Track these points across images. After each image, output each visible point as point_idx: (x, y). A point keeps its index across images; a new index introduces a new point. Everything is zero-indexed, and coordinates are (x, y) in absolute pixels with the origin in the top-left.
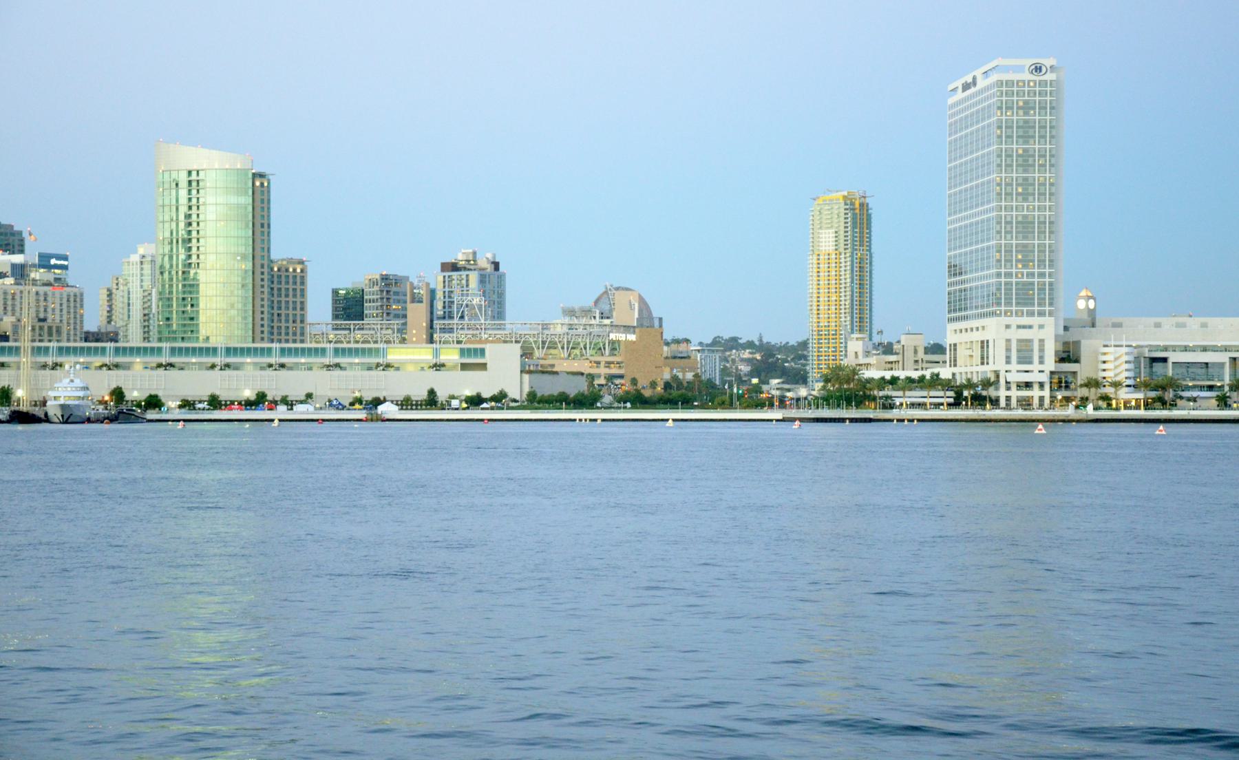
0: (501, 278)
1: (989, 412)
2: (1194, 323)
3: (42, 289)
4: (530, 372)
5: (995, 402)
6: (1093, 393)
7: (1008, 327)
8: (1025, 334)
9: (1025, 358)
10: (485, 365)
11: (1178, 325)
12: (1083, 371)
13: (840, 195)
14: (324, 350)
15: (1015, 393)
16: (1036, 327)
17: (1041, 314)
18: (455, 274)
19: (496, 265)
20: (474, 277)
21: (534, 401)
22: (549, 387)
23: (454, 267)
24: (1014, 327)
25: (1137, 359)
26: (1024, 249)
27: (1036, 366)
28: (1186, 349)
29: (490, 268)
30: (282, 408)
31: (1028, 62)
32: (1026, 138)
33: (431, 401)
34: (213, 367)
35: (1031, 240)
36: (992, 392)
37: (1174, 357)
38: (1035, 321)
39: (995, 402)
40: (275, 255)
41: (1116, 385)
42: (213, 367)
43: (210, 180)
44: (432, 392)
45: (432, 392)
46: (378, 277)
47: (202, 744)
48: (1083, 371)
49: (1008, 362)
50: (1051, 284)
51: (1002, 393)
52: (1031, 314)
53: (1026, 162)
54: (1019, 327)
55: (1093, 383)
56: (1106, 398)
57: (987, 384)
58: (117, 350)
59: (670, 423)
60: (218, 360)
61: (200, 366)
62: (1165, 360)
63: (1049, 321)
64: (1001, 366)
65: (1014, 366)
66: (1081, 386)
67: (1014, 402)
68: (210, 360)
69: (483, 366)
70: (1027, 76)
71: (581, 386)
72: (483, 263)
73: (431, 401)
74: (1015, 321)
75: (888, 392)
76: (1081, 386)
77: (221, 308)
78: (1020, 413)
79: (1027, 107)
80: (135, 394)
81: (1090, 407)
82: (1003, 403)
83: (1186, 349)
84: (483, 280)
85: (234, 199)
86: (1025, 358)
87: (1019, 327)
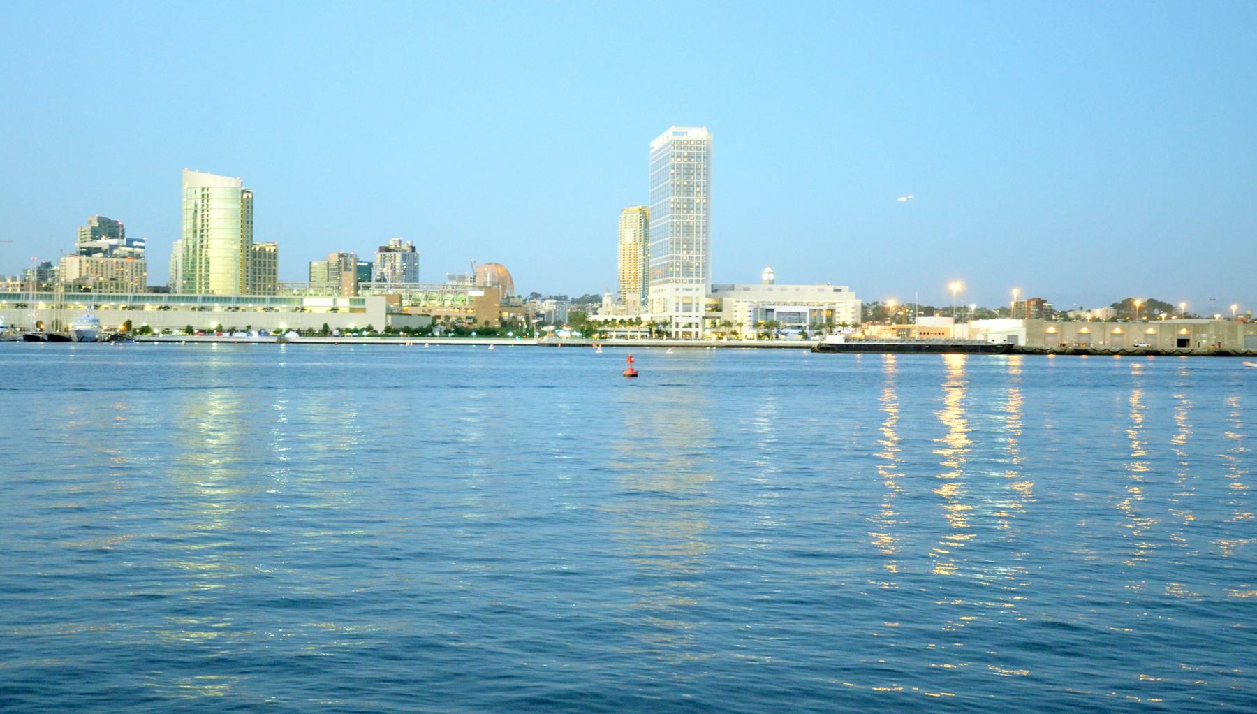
0: (416, 259)
1: (665, 341)
2: (791, 288)
3: (120, 260)
4: (392, 314)
5: (669, 335)
6: (728, 330)
9: (687, 308)
10: (364, 310)
11: (783, 290)
12: (725, 316)
13: (637, 208)
14: (126, 298)
15: (681, 330)
17: (697, 282)
18: (388, 254)
19: (413, 249)
20: (399, 256)
21: (390, 331)
22: (403, 322)
23: (387, 250)
25: (756, 309)
26: (688, 243)
27: (694, 313)
28: (785, 304)
29: (409, 250)
30: (227, 334)
32: (688, 175)
33: (326, 331)
34: (193, 309)
35: (692, 236)
36: (668, 329)
37: (777, 309)
38: (694, 286)
39: (669, 335)
41: (741, 325)
42: (193, 309)
43: (214, 193)
44: (326, 326)
45: (326, 326)
47: (363, 608)
48: (725, 316)
51: (673, 330)
52: (691, 282)
53: (689, 189)
55: (728, 324)
56: (735, 333)
57: (665, 324)
58: (169, 298)
59: (491, 347)
60: (197, 305)
61: (186, 307)
62: (772, 310)
63: (702, 286)
64: (674, 314)
65: (681, 313)
67: (680, 335)
68: (193, 305)
69: (364, 310)
71: (426, 322)
72: (405, 247)
73: (326, 331)
74: (681, 286)
75: (606, 328)
77: (223, 273)
78: (683, 342)
79: (690, 157)
80: (136, 325)
81: (725, 338)
82: (674, 335)
84: (404, 258)
85: (230, 206)
86: (687, 308)
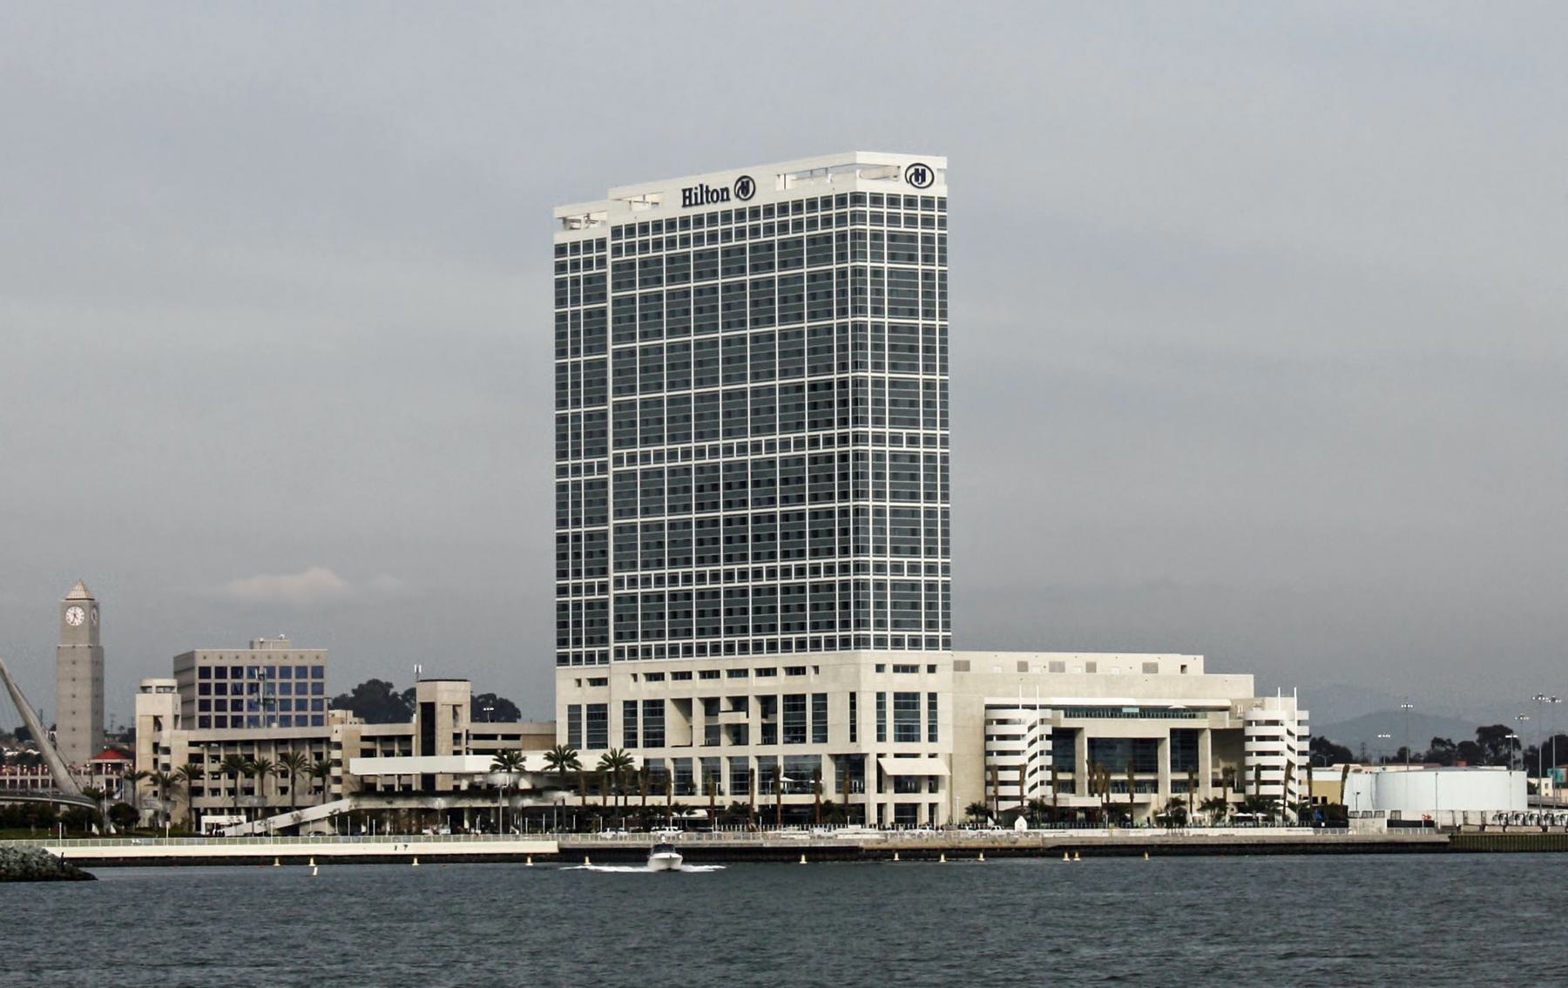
7: (880, 668)
8: (906, 683)
16: (923, 669)
17: (932, 643)
24: (889, 669)
31: (905, 160)
38: (922, 657)
40: (1251, 677)
46: (1474, 738)
49: (881, 738)
50: (946, 587)
52: (915, 643)
54: (897, 669)
65: (891, 746)
66: (340, 703)
70: (903, 189)
76: (340, 703)
81: (1021, 823)
83: (1115, 712)
87: (897, 669)
